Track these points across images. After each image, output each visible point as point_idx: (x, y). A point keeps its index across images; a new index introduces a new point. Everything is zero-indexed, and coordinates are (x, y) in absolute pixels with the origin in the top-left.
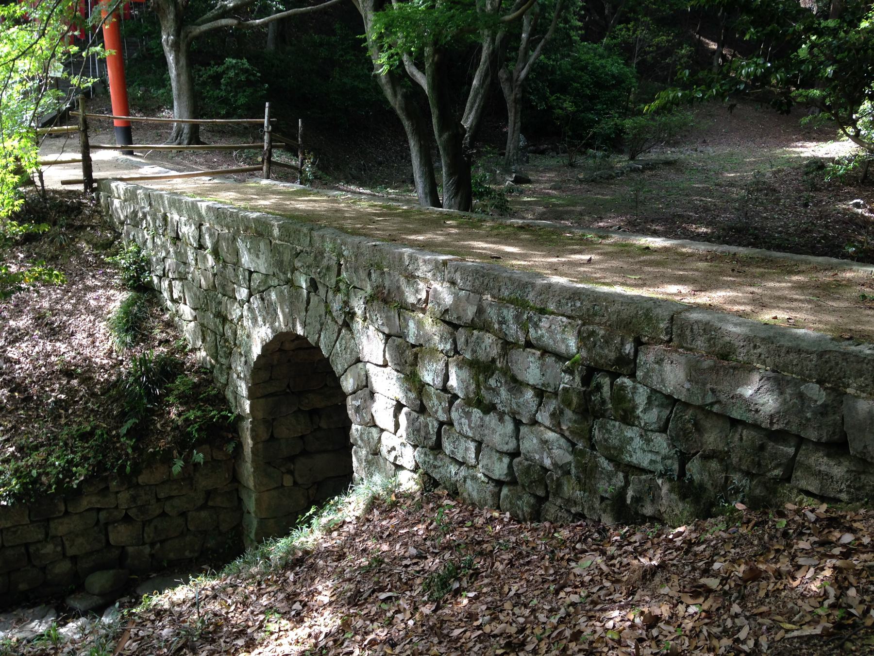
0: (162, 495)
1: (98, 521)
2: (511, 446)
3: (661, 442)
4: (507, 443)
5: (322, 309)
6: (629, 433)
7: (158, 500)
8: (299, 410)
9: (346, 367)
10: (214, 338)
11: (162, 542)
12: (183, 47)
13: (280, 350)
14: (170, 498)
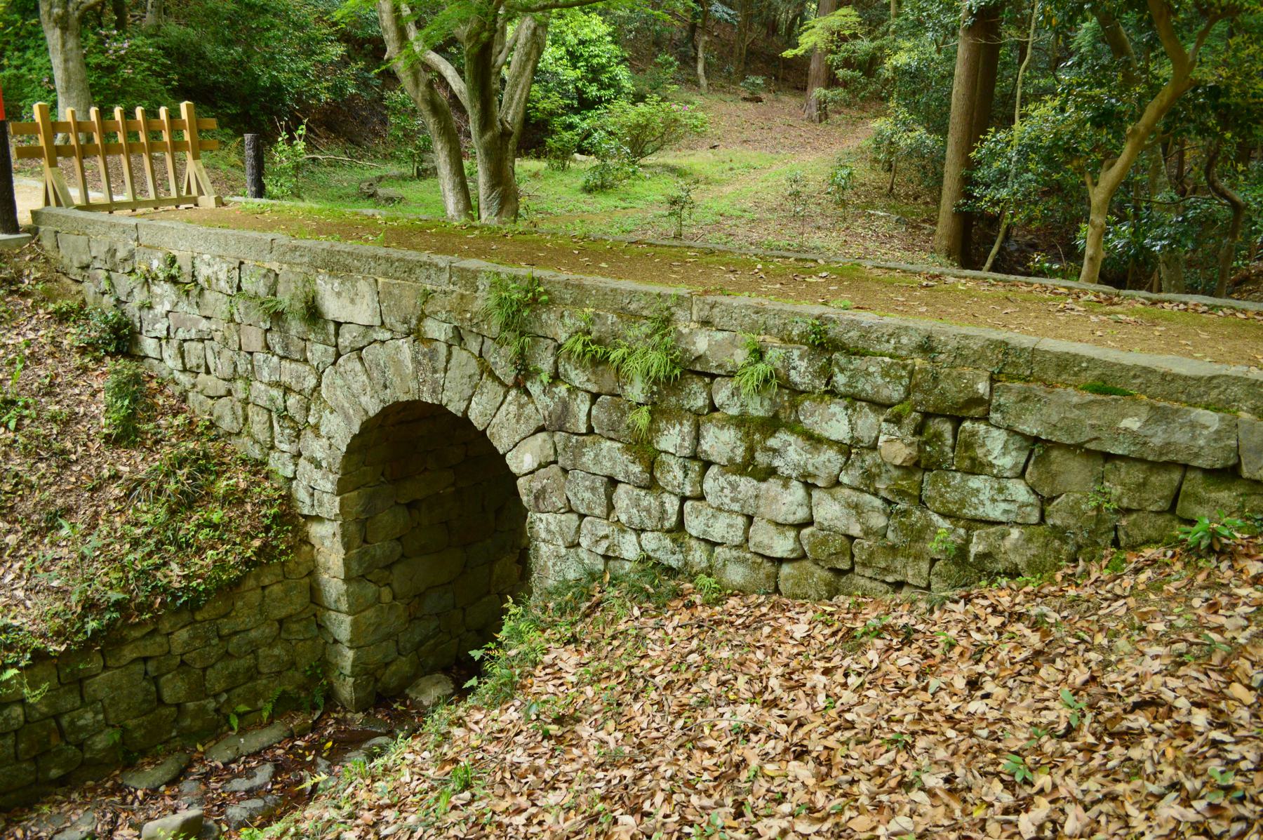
0: (225, 631)
2: (801, 514)
3: (1019, 491)
5: (473, 367)
6: (975, 482)
8: (396, 503)
9: (517, 439)
10: (266, 417)
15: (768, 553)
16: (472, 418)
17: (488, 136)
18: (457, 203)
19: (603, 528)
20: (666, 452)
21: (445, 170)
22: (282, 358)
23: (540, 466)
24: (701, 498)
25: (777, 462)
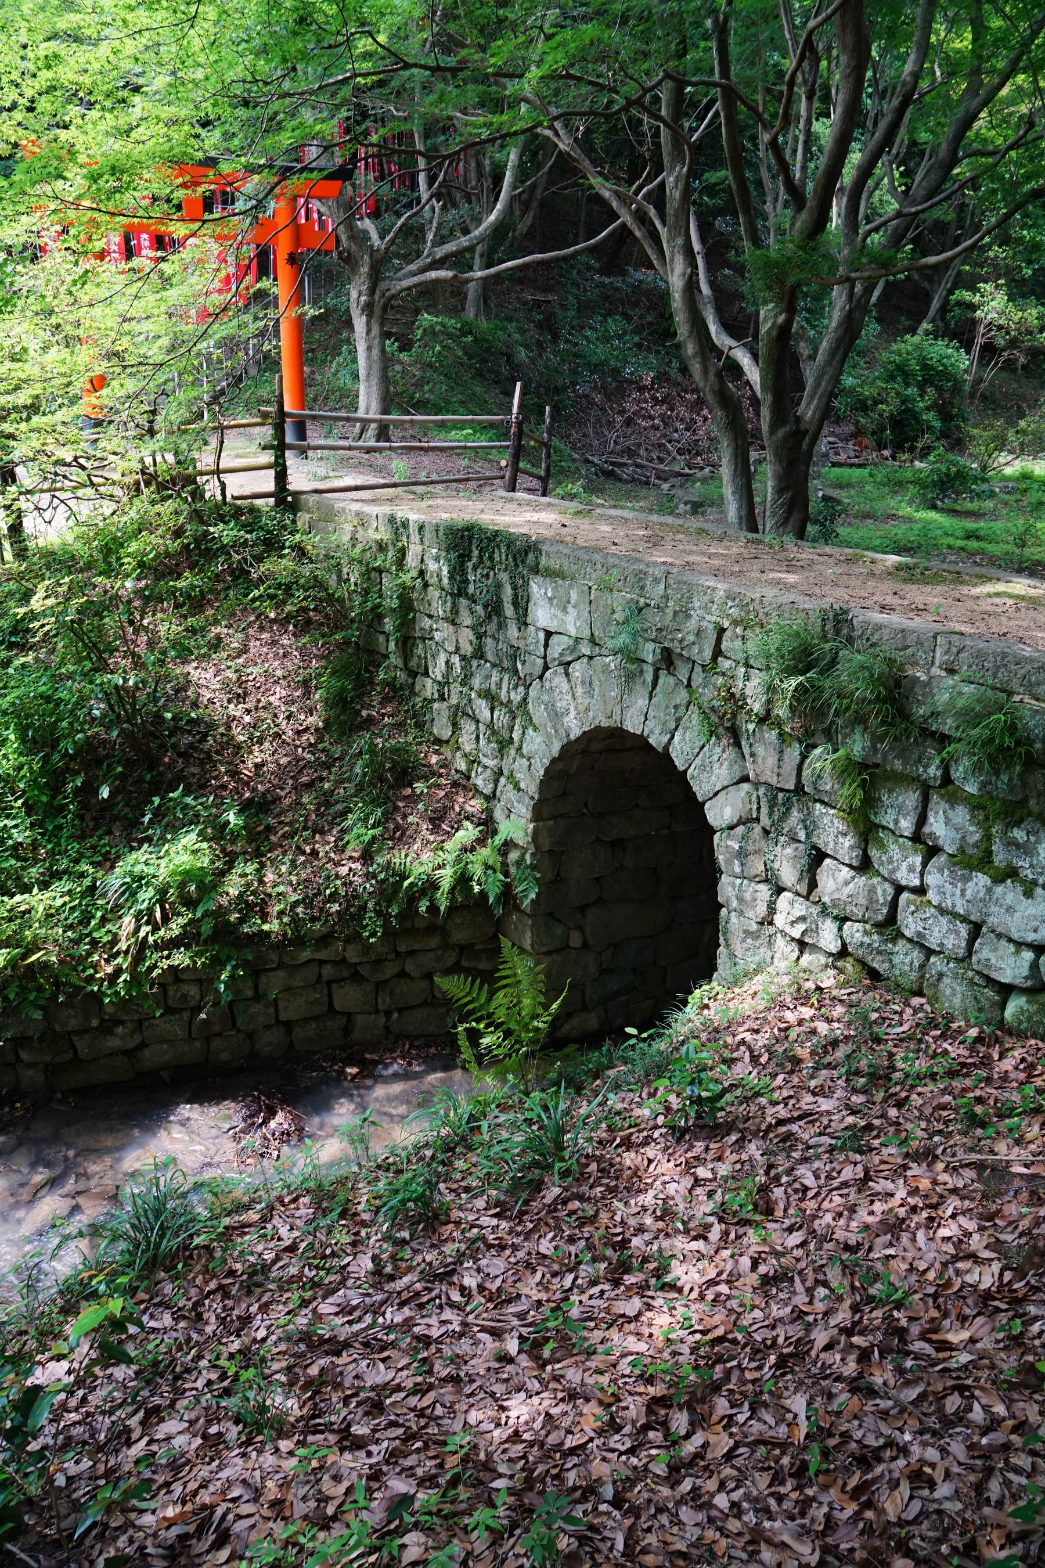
0: (402, 948)
1: (320, 976)
4: (1035, 931)
7: (398, 954)
8: (598, 839)
11: (400, 1011)
12: (378, 310)
13: (584, 752)
14: (412, 953)
15: (994, 975)
16: (673, 755)
17: (781, 433)
18: (739, 509)
19: (800, 908)
20: (884, 828)
21: (726, 472)
22: (494, 666)
23: (741, 822)
24: (921, 890)
25: (1022, 863)
